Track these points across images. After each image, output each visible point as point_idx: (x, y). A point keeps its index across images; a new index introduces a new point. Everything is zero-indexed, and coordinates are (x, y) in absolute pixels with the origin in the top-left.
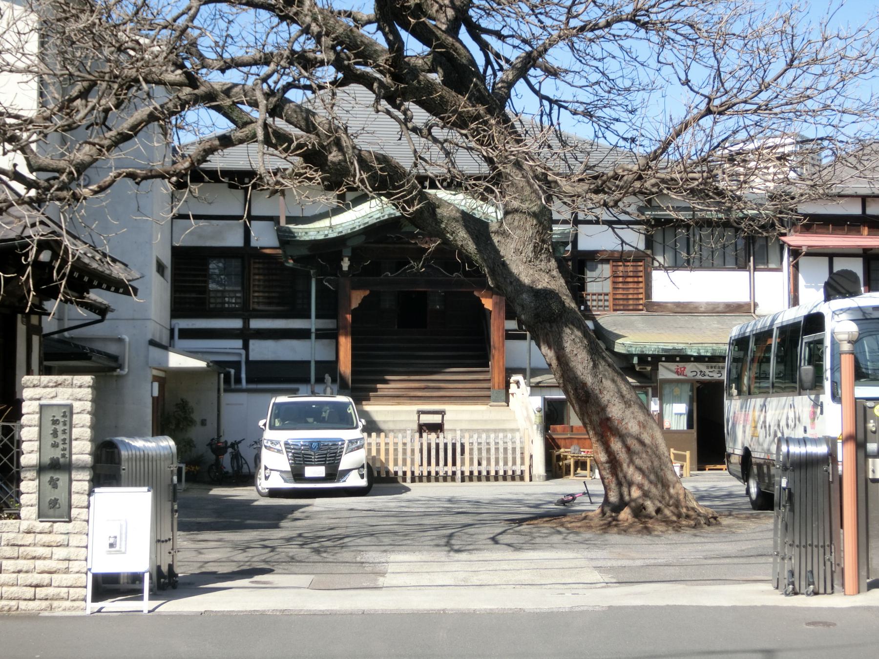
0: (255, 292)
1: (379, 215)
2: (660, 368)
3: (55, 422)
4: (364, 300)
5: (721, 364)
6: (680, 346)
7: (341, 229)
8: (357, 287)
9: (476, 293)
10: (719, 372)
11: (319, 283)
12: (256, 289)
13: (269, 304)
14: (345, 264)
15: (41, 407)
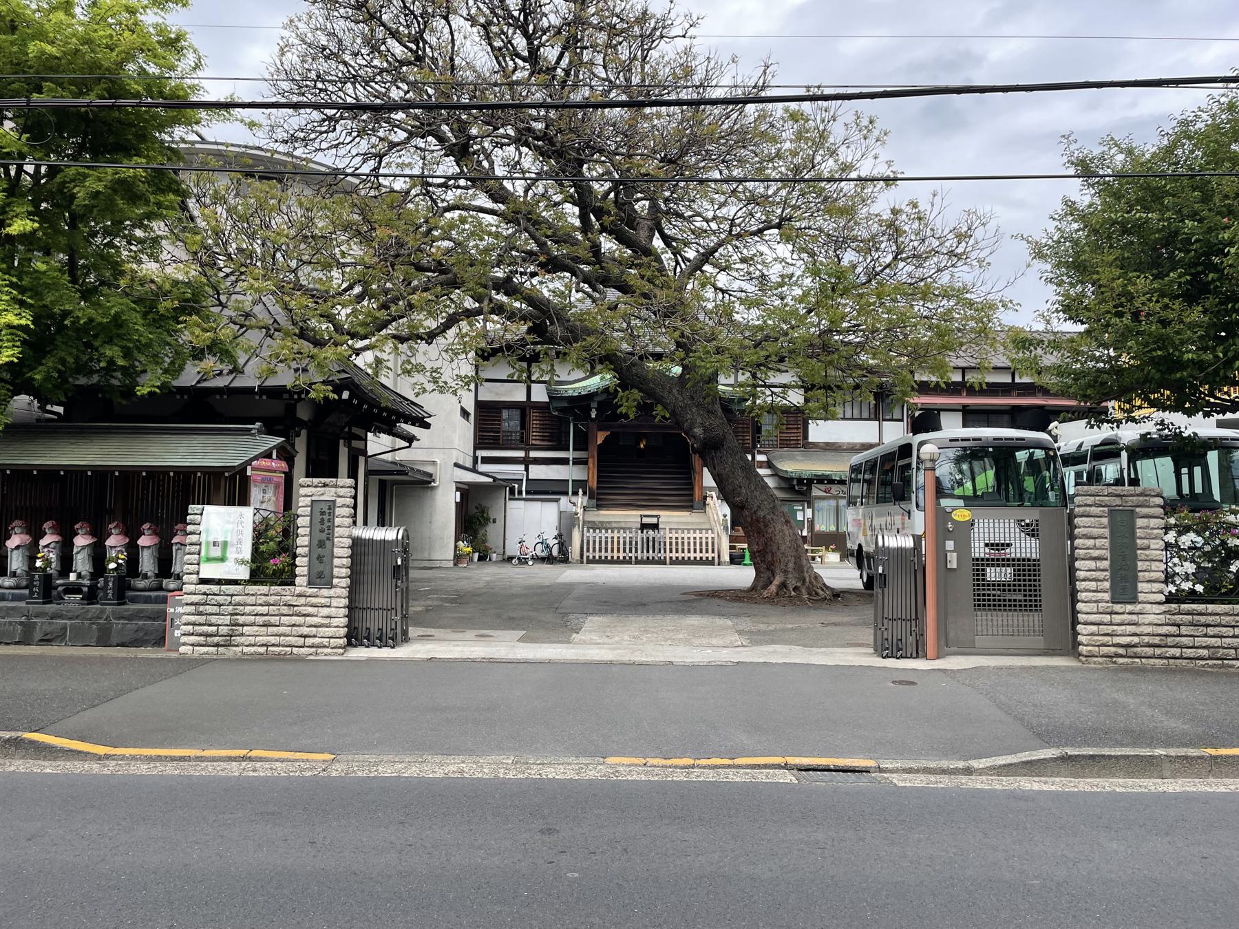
3: (323, 513)
5: (534, 437)
15: (313, 501)
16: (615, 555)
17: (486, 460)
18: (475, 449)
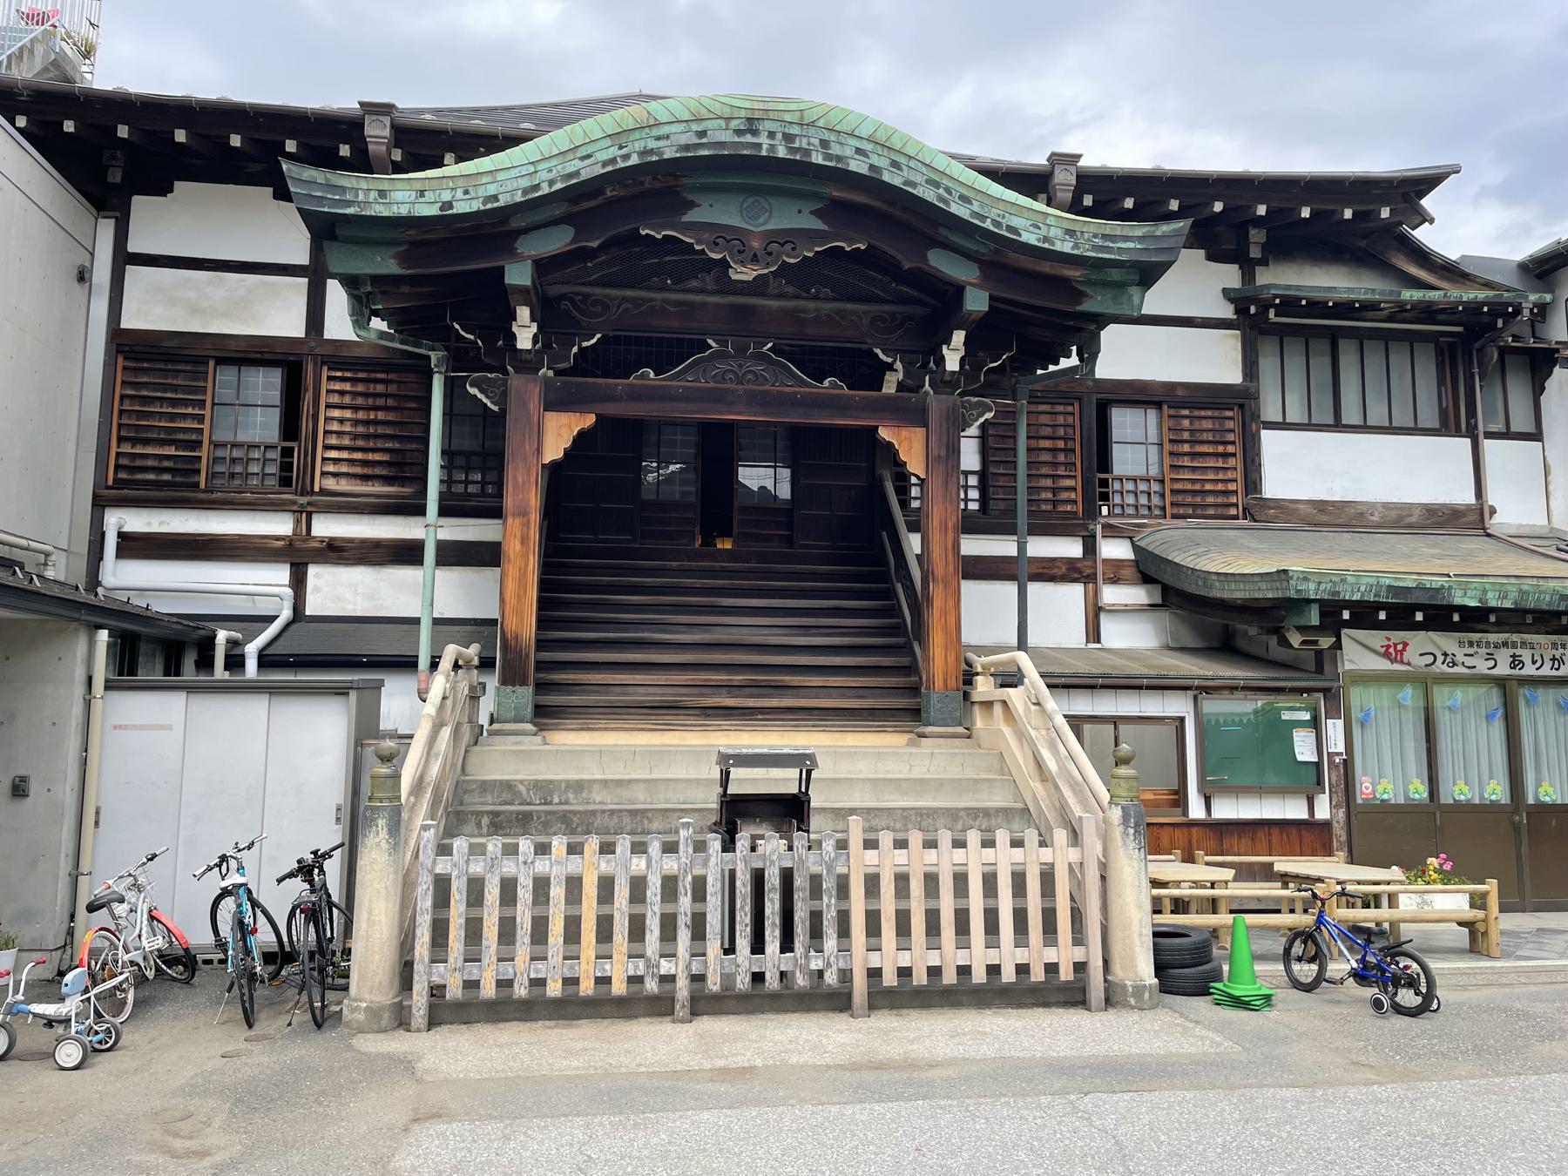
0: (327, 447)
1: (613, 152)
2: (1345, 640)
4: (582, 438)
6: (1438, 582)
8: (557, 402)
9: (884, 433)
10: (1490, 657)
11: (453, 390)
12: (333, 441)
13: (365, 478)
14: (525, 335)
16: (587, 970)
17: (135, 546)
18: (100, 503)
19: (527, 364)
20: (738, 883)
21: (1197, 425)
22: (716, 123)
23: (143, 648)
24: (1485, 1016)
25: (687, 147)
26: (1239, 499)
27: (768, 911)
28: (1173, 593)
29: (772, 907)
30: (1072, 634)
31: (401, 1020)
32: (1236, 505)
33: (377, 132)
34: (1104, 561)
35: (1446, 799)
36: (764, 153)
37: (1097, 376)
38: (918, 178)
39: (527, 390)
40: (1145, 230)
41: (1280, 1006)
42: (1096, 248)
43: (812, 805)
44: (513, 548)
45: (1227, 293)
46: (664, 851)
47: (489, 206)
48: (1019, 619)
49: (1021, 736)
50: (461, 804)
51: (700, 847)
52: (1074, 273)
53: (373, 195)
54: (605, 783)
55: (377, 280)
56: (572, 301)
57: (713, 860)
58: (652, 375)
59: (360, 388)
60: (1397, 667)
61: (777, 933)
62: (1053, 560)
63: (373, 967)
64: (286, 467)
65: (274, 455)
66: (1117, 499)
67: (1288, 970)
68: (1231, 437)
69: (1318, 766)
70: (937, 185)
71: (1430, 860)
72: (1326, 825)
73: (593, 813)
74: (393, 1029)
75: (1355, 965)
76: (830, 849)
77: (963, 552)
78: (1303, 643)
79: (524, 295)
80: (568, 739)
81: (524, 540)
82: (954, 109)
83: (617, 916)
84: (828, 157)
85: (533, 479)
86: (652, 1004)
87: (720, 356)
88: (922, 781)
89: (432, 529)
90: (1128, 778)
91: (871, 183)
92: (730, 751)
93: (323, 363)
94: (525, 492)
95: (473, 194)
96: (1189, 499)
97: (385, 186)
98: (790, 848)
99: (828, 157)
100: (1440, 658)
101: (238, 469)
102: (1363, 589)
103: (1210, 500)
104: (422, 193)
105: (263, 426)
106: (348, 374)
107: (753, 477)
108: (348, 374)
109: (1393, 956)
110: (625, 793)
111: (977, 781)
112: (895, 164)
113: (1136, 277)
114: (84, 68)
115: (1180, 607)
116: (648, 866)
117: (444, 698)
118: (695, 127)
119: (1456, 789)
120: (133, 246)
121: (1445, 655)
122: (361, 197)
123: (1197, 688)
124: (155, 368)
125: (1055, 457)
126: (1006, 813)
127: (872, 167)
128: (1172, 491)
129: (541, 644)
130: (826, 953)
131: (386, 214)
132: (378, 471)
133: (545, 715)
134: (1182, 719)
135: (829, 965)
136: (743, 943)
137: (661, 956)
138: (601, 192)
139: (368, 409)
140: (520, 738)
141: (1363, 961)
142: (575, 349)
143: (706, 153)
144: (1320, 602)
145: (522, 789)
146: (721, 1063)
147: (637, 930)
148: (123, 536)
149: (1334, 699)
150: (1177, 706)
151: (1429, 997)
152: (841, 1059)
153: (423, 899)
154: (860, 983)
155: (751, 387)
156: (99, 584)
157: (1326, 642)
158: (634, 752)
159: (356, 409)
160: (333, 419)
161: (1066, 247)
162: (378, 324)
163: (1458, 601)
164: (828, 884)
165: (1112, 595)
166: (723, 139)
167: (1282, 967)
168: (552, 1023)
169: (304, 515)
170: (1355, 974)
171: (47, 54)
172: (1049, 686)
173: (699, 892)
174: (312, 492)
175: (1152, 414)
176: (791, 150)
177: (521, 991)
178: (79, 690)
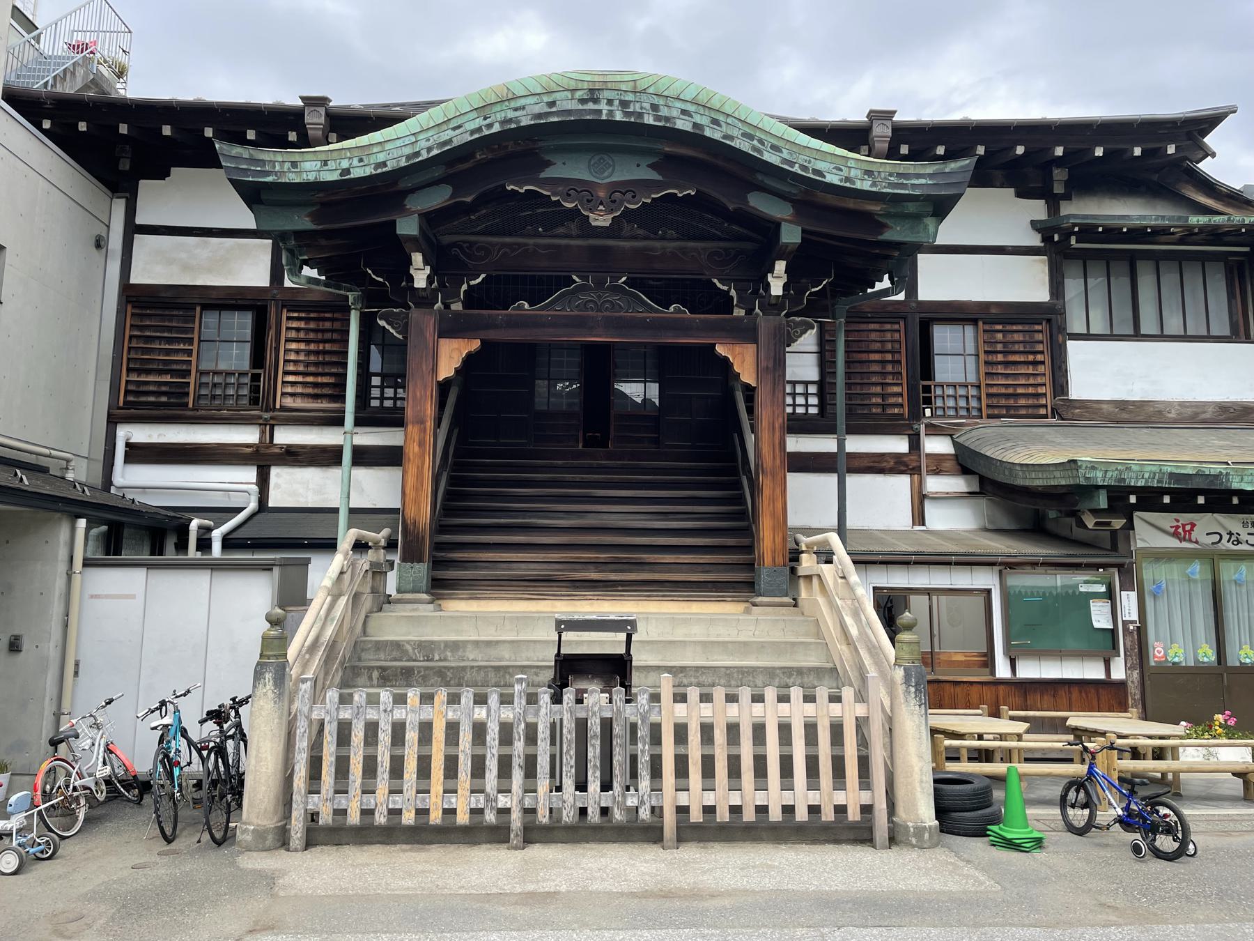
0: (286, 373)
1: (479, 122)
2: (1136, 522)
4: (469, 360)
6: (1216, 469)
7: (381, 157)
8: (451, 328)
9: (721, 350)
11: (367, 326)
12: (291, 368)
13: (315, 397)
16: (436, 802)
17: (139, 454)
18: (113, 421)
19: (424, 300)
20: (565, 731)
21: (1009, 338)
22: (562, 95)
23: (126, 532)
24: (1238, 861)
25: (539, 116)
26: (1048, 401)
27: (590, 755)
28: (989, 483)
29: (594, 752)
30: (901, 518)
31: (282, 840)
32: (1046, 406)
33: (315, 120)
34: (928, 455)
35: (1232, 661)
36: (604, 117)
37: (920, 298)
38: (735, 133)
39: (424, 321)
40: (935, 167)
41: (1051, 848)
42: (892, 185)
43: (634, 663)
44: (413, 450)
45: (1035, 225)
46: (502, 703)
47: (379, 171)
48: (856, 508)
49: (831, 604)
50: (360, 660)
51: (532, 699)
52: (875, 208)
53: (287, 165)
54: (476, 643)
55: (299, 234)
56: (461, 248)
57: (543, 711)
58: (527, 306)
59: (312, 325)
60: (1185, 545)
61: (598, 774)
62: (883, 455)
63: (260, 796)
64: (255, 389)
65: (247, 380)
66: (939, 403)
67: (1064, 813)
68: (1040, 347)
69: (1113, 632)
70: (751, 137)
71: (1216, 716)
72: (1122, 685)
73: (464, 668)
74: (276, 848)
75: (1120, 813)
76: (644, 702)
77: (788, 450)
78: (1097, 524)
79: (416, 244)
80: (458, 606)
81: (421, 444)
82: (788, 84)
83: (461, 757)
84: (658, 118)
85: (429, 393)
86: (485, 832)
87: (582, 289)
88: (745, 644)
89: (348, 436)
90: (910, 643)
91: (695, 138)
92: (564, 617)
93: (283, 306)
94: (420, 402)
95: (366, 162)
96: (1003, 402)
97: (297, 158)
98: (611, 702)
99: (658, 118)
100: (1226, 537)
101: (219, 392)
102: (1146, 476)
103: (1022, 402)
104: (325, 163)
105: (237, 358)
106: (303, 315)
107: (633, 390)
108: (303, 315)
109: (1154, 805)
110: (493, 652)
111: (793, 644)
112: (715, 122)
113: (930, 209)
114: (119, 86)
115: (994, 495)
116: (488, 715)
117: (342, 573)
118: (546, 99)
119: (1242, 653)
120: (140, 220)
121: (1230, 534)
122: (277, 168)
123: (1001, 564)
124: (155, 315)
125: (884, 368)
126: (818, 671)
127: (695, 125)
128: (988, 395)
129: (440, 528)
130: (641, 792)
131: (297, 180)
132: (326, 391)
133: (440, 587)
134: (989, 591)
135: (643, 802)
136: (569, 783)
137: (499, 791)
138: (472, 155)
139: (317, 342)
140: (416, 606)
141: (1127, 809)
142: (464, 287)
143: (556, 119)
144: (1108, 488)
145: (409, 648)
146: (531, 887)
147: (478, 769)
148: (128, 445)
149: (1128, 576)
150: (985, 579)
151: (1184, 843)
152: (635, 887)
153: (301, 741)
154: (669, 819)
155: (608, 314)
156: (111, 483)
157: (1118, 523)
158: (503, 618)
159: (308, 342)
160: (291, 350)
161: (866, 185)
162: (307, 271)
163: (1235, 485)
164: (643, 732)
165: (934, 484)
166: (569, 108)
167: (1057, 811)
168: (408, 847)
169: (268, 427)
170: (1120, 820)
171: (86, 74)
172: (855, 562)
173: (531, 738)
174: (275, 409)
175: (969, 330)
176: (627, 114)
177: (381, 819)
178: (62, 568)
